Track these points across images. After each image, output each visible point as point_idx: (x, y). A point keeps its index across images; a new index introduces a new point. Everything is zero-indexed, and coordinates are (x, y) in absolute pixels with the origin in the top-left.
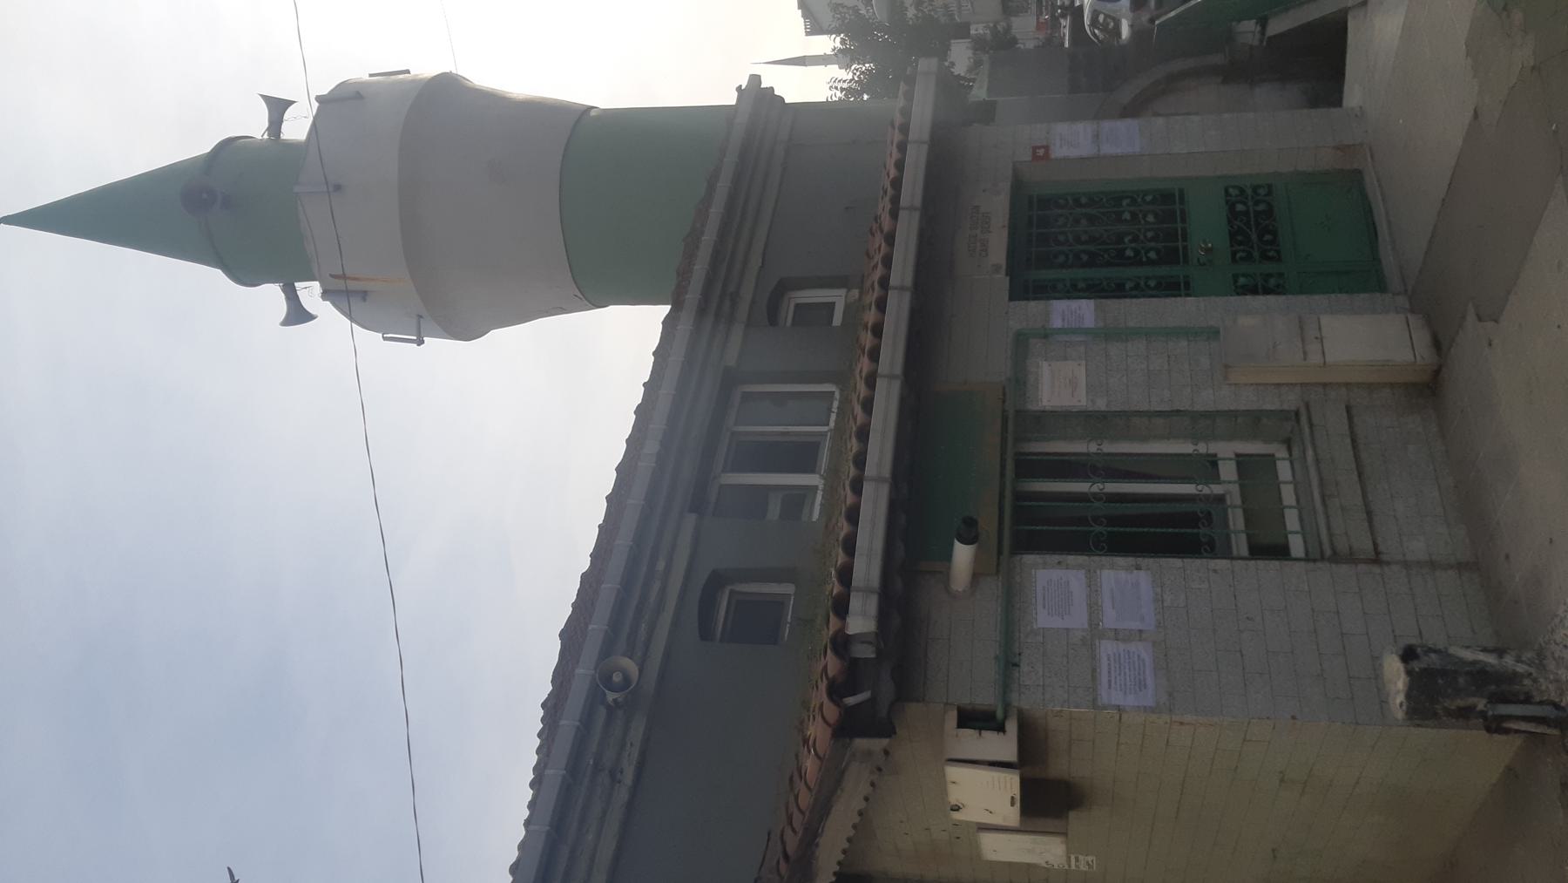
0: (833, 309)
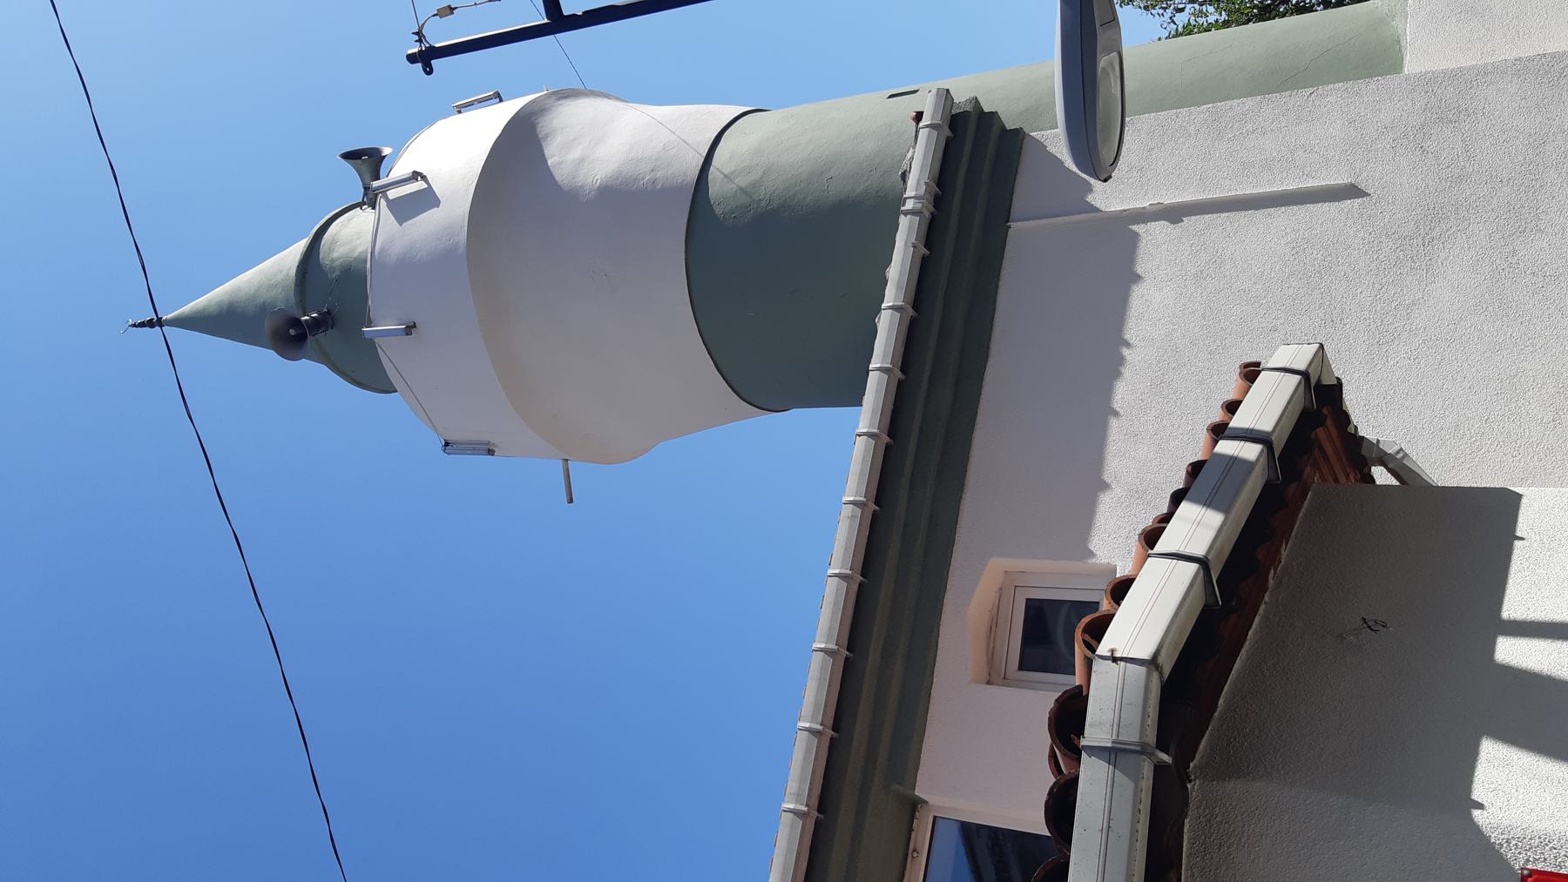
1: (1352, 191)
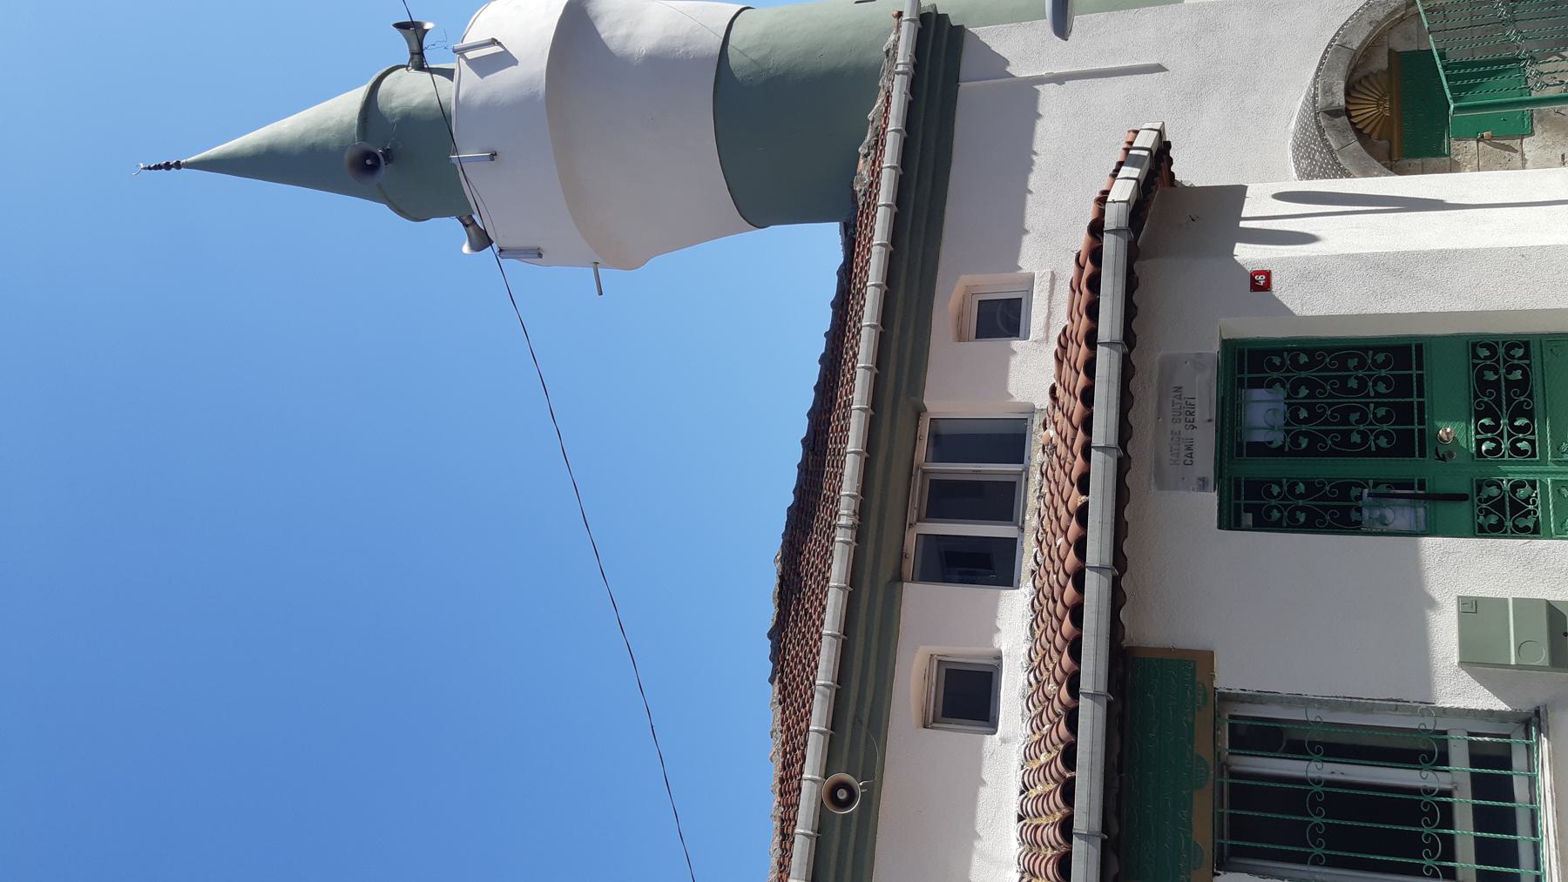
0: (1015, 486)
1: (1159, 68)
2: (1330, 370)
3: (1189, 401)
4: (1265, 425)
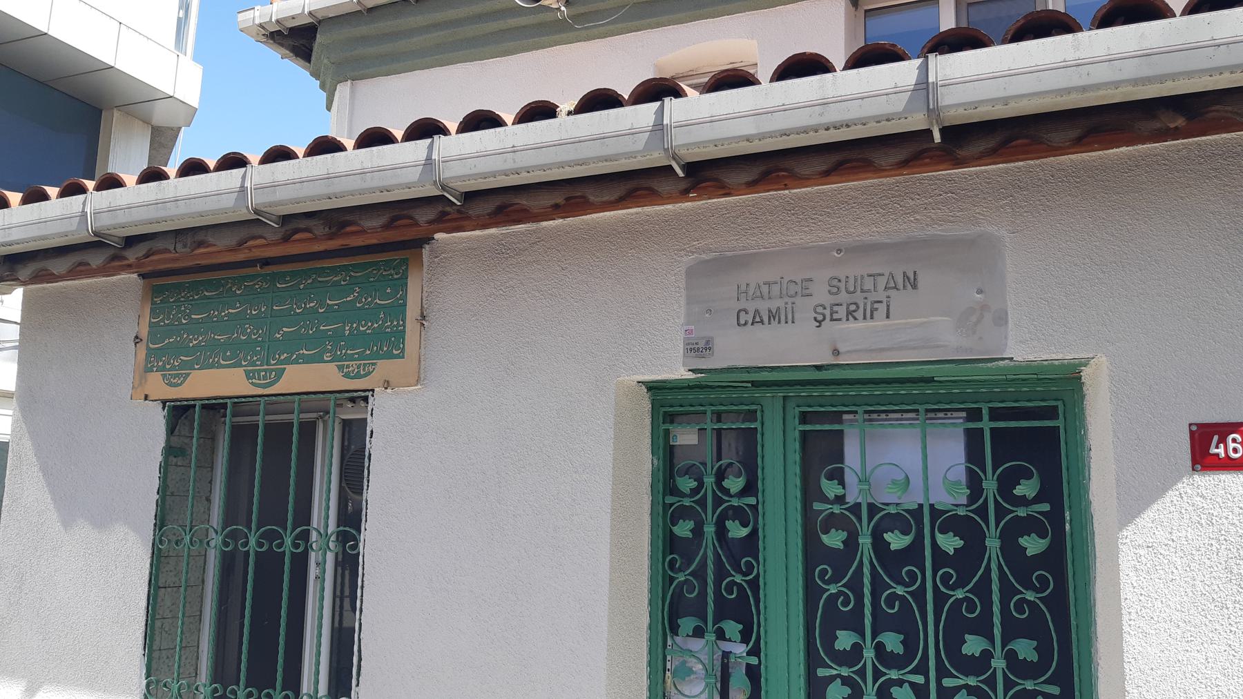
2: (718, 584)
3: (882, 308)
4: (868, 470)
